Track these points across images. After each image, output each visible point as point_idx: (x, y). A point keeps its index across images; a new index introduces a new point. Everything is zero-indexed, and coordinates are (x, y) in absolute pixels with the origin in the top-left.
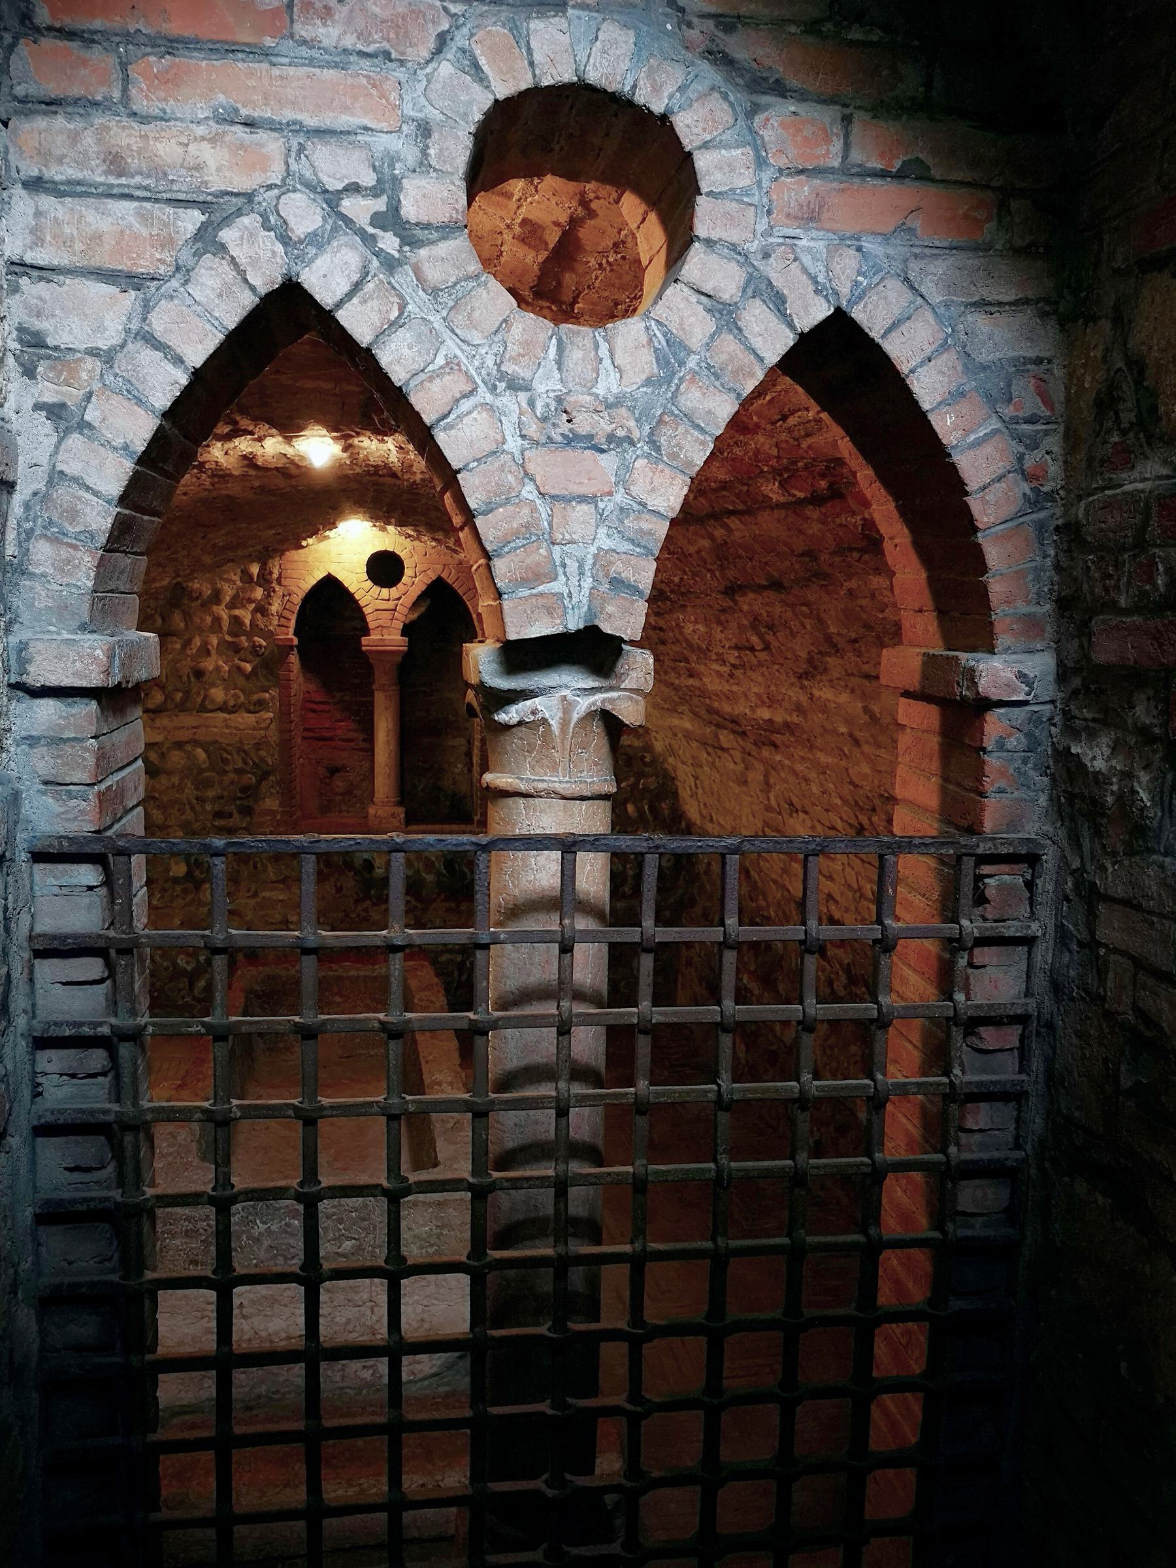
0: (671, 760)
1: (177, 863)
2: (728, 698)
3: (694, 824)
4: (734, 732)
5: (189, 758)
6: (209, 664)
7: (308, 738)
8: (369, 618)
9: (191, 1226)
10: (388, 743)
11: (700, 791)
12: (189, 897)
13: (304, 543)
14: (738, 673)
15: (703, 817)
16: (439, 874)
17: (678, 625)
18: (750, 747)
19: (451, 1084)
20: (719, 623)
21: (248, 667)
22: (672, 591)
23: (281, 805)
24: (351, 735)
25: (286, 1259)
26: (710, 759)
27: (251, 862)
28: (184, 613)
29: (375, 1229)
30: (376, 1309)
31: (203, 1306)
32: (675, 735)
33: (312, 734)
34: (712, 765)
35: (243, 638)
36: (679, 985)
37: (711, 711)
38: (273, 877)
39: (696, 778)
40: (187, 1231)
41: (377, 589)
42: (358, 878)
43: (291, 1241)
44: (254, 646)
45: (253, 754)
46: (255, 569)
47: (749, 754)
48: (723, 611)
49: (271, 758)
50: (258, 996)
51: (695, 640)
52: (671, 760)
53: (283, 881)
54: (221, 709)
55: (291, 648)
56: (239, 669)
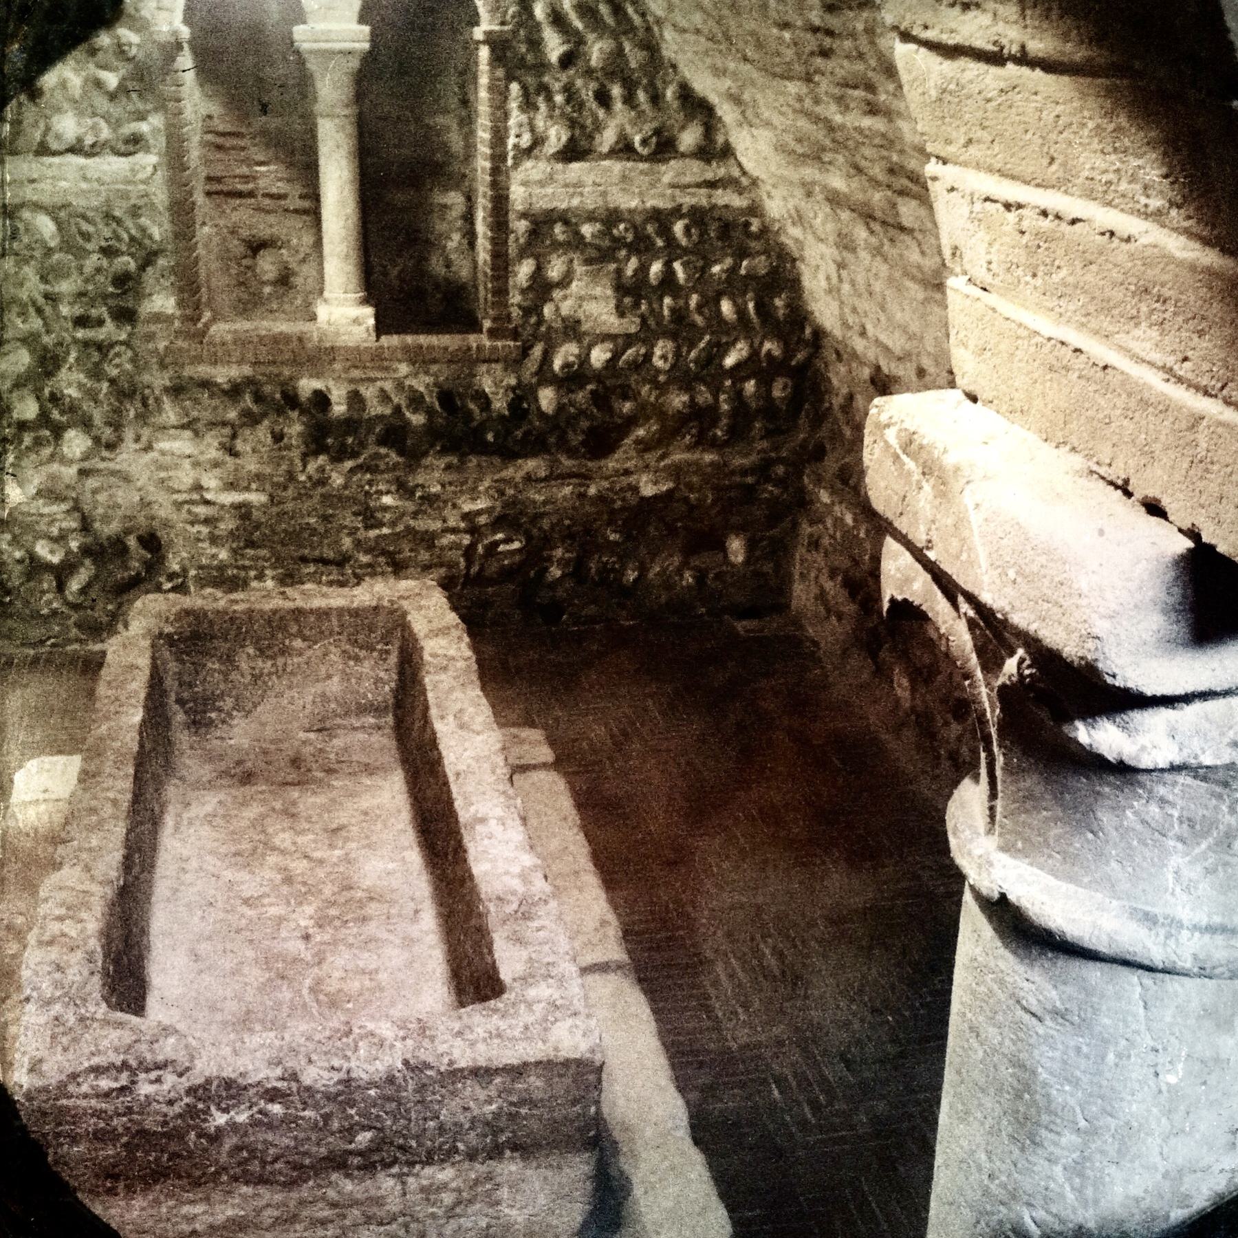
0: (795, 232)
7: (217, 193)
9: (102, 1125)
10: (342, 203)
11: (846, 287)
12: (47, 452)
15: (845, 325)
19: (502, 821)
24: (280, 187)
25: (264, 1163)
26: (873, 240)
27: (138, 397)
34: (877, 252)
39: (841, 266)
43: (270, 1137)
45: (129, 223)
49: (158, 230)
54: (72, 150)
56: (99, 84)
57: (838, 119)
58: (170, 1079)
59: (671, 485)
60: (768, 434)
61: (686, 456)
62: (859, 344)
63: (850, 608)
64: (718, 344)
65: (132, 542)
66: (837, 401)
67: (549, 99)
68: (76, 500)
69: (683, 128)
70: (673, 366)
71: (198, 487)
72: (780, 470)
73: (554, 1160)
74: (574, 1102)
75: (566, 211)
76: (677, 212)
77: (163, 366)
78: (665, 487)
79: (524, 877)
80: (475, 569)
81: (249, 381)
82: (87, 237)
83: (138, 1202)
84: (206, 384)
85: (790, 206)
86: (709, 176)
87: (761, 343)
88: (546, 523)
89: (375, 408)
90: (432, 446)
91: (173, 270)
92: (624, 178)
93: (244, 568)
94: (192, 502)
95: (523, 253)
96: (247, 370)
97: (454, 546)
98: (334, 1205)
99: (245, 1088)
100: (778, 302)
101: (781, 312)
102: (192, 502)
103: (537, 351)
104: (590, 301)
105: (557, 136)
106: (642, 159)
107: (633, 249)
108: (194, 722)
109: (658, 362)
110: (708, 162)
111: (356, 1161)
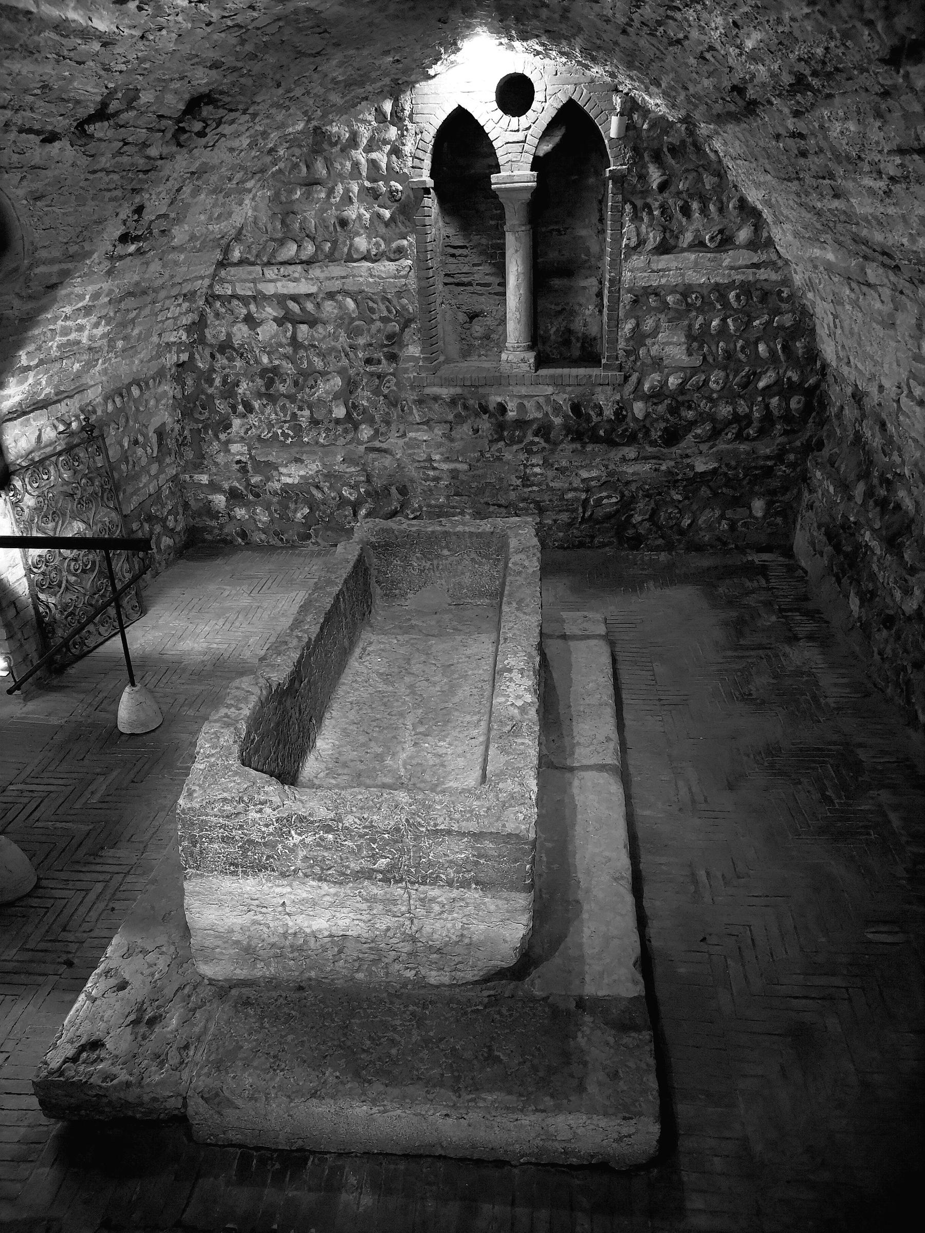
1: (337, 406)
2: (880, 224)
3: (829, 365)
4: (884, 265)
5: (340, 308)
6: (351, 213)
8: (499, 153)
10: (518, 286)
11: (839, 331)
12: (349, 437)
13: (431, 72)
14: (898, 188)
16: (566, 417)
17: (822, 127)
18: (902, 283)
19: (522, 671)
20: (879, 115)
21: (387, 214)
22: (815, 74)
23: (422, 352)
24: (489, 279)
25: (322, 869)
26: (853, 296)
28: (326, 159)
29: (409, 850)
30: (415, 921)
31: (249, 901)
32: (816, 267)
33: (450, 280)
34: (855, 304)
35: (381, 183)
36: (798, 527)
37: (857, 239)
38: (418, 419)
39: (835, 317)
40: (223, 838)
41: (507, 118)
42: (493, 420)
43: (326, 854)
44: (391, 192)
46: (388, 106)
47: (901, 292)
48: (886, 94)
49: (412, 307)
50: (374, 548)
51: (843, 146)
52: (810, 295)
53: (426, 423)
54: (365, 258)
55: (427, 191)
56: (379, 216)
57: (819, 205)
58: (268, 810)
59: (716, 465)
60: (786, 433)
61: (730, 447)
62: (845, 370)
63: (829, 549)
64: (754, 373)
65: (393, 490)
66: (834, 410)
67: (650, 212)
68: (364, 465)
69: (739, 229)
70: (723, 388)
71: (430, 460)
72: (792, 457)
73: (505, 894)
74: (516, 861)
75: (658, 287)
76: (731, 285)
77: (413, 388)
78: (712, 466)
79: (523, 710)
80: (588, 514)
81: (461, 396)
82: (372, 311)
83: (251, 881)
84: (436, 398)
85: (806, 277)
86: (755, 260)
87: (785, 372)
88: (633, 487)
89: (533, 414)
90: (566, 435)
91: (419, 330)
92: (696, 263)
93: (453, 507)
94: (425, 468)
95: (627, 317)
96: (459, 390)
97: (577, 499)
98: (367, 900)
99: (312, 823)
100: (798, 344)
101: (800, 351)
102: (425, 468)
103: (634, 378)
104: (671, 346)
105: (653, 238)
106: (710, 250)
107: (700, 310)
108: (386, 595)
109: (712, 385)
110: (756, 252)
111: (380, 876)
